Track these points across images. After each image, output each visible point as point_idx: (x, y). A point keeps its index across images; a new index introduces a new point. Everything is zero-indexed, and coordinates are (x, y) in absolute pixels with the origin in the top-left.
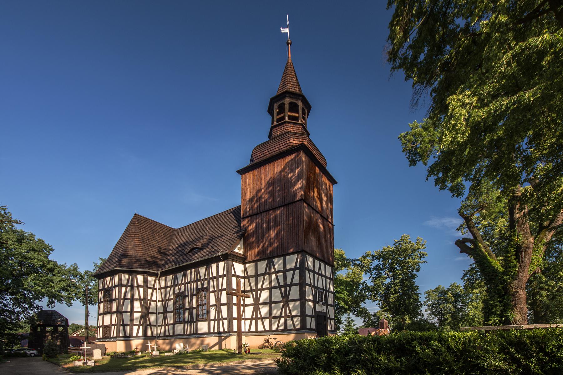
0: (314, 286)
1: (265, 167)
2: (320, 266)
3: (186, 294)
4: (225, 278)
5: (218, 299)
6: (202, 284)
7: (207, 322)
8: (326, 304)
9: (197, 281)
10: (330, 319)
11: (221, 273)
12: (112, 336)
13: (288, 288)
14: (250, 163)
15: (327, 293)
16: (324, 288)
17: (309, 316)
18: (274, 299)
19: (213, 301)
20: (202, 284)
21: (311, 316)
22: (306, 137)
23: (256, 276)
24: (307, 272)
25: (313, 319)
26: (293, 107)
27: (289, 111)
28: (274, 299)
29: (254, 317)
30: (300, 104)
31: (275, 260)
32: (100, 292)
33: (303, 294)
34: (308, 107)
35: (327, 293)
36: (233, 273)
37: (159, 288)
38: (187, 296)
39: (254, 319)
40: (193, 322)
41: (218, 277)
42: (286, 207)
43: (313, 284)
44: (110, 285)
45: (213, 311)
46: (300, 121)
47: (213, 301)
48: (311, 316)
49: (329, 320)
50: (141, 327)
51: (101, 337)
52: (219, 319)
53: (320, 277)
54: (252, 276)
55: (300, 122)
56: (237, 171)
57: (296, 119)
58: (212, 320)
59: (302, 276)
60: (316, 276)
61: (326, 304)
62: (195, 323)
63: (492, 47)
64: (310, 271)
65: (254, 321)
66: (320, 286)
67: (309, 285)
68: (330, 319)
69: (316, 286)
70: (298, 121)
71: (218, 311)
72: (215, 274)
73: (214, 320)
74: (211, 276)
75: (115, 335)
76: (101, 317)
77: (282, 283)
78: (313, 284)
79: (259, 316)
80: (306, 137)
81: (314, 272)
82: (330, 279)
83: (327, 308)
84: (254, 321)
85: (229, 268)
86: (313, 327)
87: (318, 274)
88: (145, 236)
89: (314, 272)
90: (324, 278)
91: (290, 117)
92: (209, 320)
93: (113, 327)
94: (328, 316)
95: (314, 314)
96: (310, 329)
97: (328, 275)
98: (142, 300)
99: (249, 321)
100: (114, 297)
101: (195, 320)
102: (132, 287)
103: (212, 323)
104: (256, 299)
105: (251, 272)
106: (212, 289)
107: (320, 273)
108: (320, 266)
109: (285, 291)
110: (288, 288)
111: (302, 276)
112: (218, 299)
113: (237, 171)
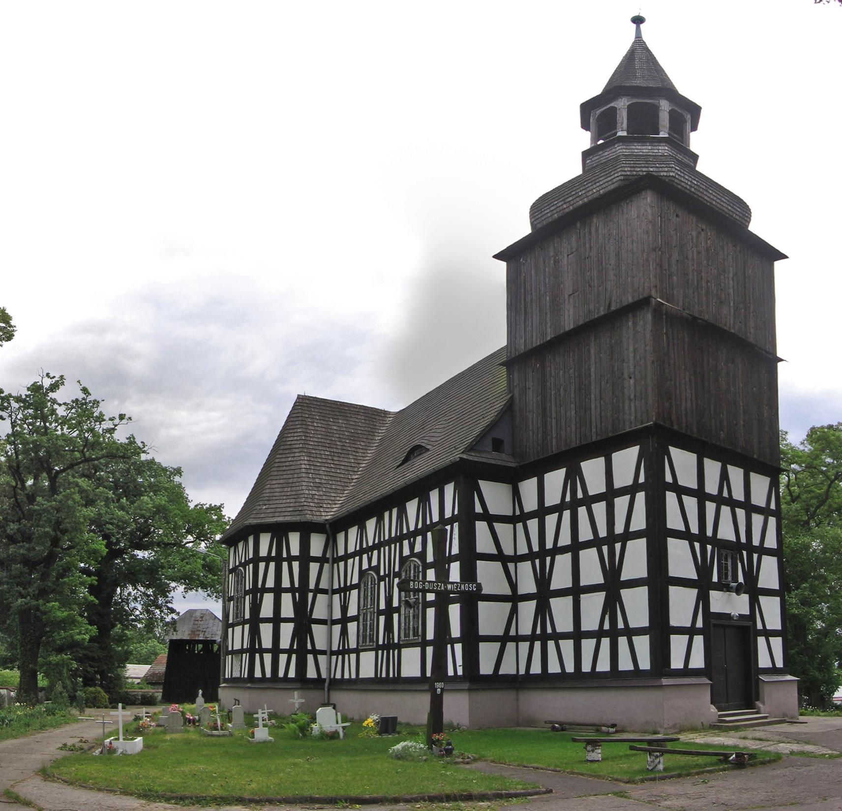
0: (702, 537)
7: (776, 586)
8: (754, 592)
9: (400, 539)
10: (768, 634)
11: (448, 514)
15: (755, 556)
16: (743, 539)
17: (680, 631)
21: (691, 632)
25: (699, 640)
32: (231, 575)
35: (755, 556)
36: (669, 478)
37: (328, 562)
41: (542, 512)
43: (695, 529)
44: (243, 561)
48: (691, 632)
49: (761, 641)
50: (294, 656)
56: (496, 257)
59: (656, 511)
60: (710, 507)
61: (754, 592)
64: (681, 491)
65: (538, 645)
67: (684, 535)
68: (768, 634)
78: (695, 529)
82: (765, 512)
83: (754, 603)
86: (698, 661)
87: (719, 500)
90: (741, 513)
94: (759, 626)
95: (700, 624)
96: (686, 672)
98: (297, 590)
102: (279, 560)
104: (543, 580)
111: (656, 511)
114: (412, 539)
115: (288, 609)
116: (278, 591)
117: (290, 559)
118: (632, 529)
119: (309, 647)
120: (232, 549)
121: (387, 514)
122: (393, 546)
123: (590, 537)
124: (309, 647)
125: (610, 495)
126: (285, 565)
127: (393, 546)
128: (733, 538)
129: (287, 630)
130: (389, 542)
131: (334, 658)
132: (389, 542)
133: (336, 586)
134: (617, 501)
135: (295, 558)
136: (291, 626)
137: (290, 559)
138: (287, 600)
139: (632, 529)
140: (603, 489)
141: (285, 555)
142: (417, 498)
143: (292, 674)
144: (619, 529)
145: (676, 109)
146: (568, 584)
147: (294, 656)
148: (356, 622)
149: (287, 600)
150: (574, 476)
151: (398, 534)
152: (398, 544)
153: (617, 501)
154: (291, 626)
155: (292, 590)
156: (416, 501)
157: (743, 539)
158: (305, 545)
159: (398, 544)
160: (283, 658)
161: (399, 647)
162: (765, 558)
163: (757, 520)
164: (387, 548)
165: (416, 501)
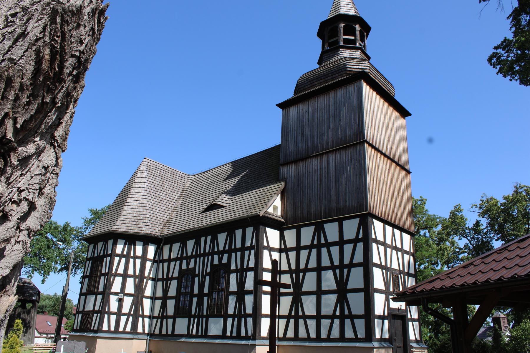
1: (294, 106)
2: (393, 235)
3: (197, 272)
4: (253, 252)
5: (241, 283)
6: (220, 259)
9: (212, 254)
12: (92, 328)
13: (346, 270)
14: (294, 95)
16: (401, 269)
18: (314, 298)
19: (233, 286)
20: (220, 259)
22: (366, 63)
23: (298, 248)
24: (374, 245)
26: (349, 30)
27: (344, 35)
28: (314, 298)
29: (293, 314)
30: (358, 27)
31: (327, 226)
32: (88, 262)
33: (368, 278)
34: (366, 29)
36: (265, 244)
38: (198, 275)
39: (293, 317)
40: (203, 316)
41: (243, 249)
42: (342, 151)
44: (101, 254)
45: (232, 301)
46: (357, 44)
47: (233, 286)
48: (382, 318)
50: (131, 318)
51: (78, 328)
52: (240, 315)
53: (394, 252)
54: (292, 249)
55: (358, 45)
56: (277, 105)
57: (354, 42)
58: (230, 316)
60: (389, 250)
62: (204, 319)
63: (458, 252)
66: (395, 266)
67: (379, 266)
69: (389, 266)
70: (356, 45)
71: (241, 302)
72: (239, 245)
73: (233, 316)
74: (233, 247)
75: (96, 328)
76: (83, 298)
77: (336, 263)
78: (383, 264)
79: (300, 314)
80: (366, 63)
81: (384, 244)
84: (292, 321)
85: (258, 237)
88: (152, 186)
89: (384, 244)
91: (345, 41)
92: (226, 316)
93: (95, 315)
94: (409, 317)
97: (407, 247)
98: (138, 277)
99: (285, 320)
100: (103, 272)
101: (205, 313)
103: (230, 320)
105: (291, 242)
106: (233, 267)
107: (394, 245)
108: (393, 235)
109: (342, 273)
110: (346, 270)
112: (241, 283)
113: (277, 105)
114: (221, 255)
115: (130, 288)
116: (125, 276)
117: (135, 257)
118: (307, 251)
119: (141, 313)
120: (92, 246)
121: (203, 239)
122: (206, 258)
123: (290, 253)
124: (141, 313)
125: (341, 243)
126: (132, 261)
127: (206, 258)
128: (398, 268)
129: (128, 302)
130: (204, 255)
131: (155, 320)
132: (204, 255)
133: (160, 276)
134: (346, 246)
135: (138, 257)
136: (131, 298)
137: (135, 257)
138: (130, 282)
139: (307, 251)
140: (337, 239)
141: (132, 255)
142: (227, 233)
143: (128, 329)
144: (347, 261)
145: (342, 31)
146: (314, 289)
147: (131, 318)
148: (82, 292)
149: (130, 282)
150: (319, 230)
151: (211, 251)
152: (210, 257)
153: (346, 246)
154: (131, 298)
155: (134, 276)
156: (225, 234)
157: (401, 269)
158: (145, 252)
159: (210, 257)
160: (123, 319)
161: (207, 317)
162: (277, 246)
163: (406, 257)
164: (202, 258)
165: (225, 234)
